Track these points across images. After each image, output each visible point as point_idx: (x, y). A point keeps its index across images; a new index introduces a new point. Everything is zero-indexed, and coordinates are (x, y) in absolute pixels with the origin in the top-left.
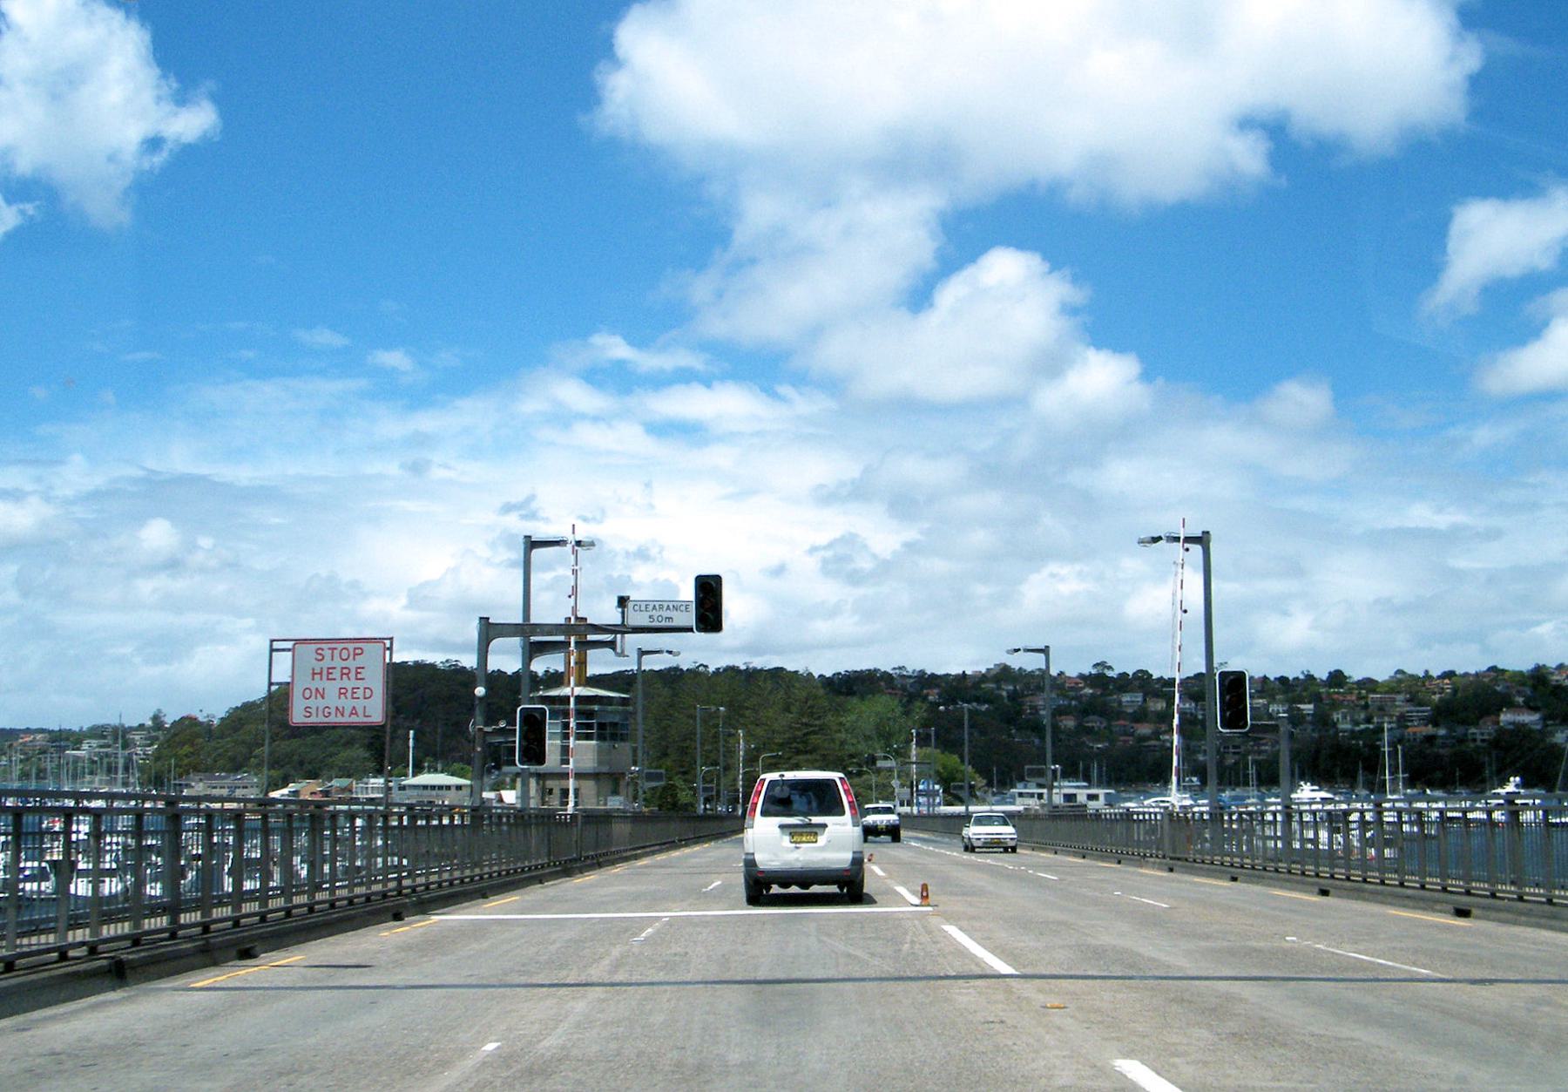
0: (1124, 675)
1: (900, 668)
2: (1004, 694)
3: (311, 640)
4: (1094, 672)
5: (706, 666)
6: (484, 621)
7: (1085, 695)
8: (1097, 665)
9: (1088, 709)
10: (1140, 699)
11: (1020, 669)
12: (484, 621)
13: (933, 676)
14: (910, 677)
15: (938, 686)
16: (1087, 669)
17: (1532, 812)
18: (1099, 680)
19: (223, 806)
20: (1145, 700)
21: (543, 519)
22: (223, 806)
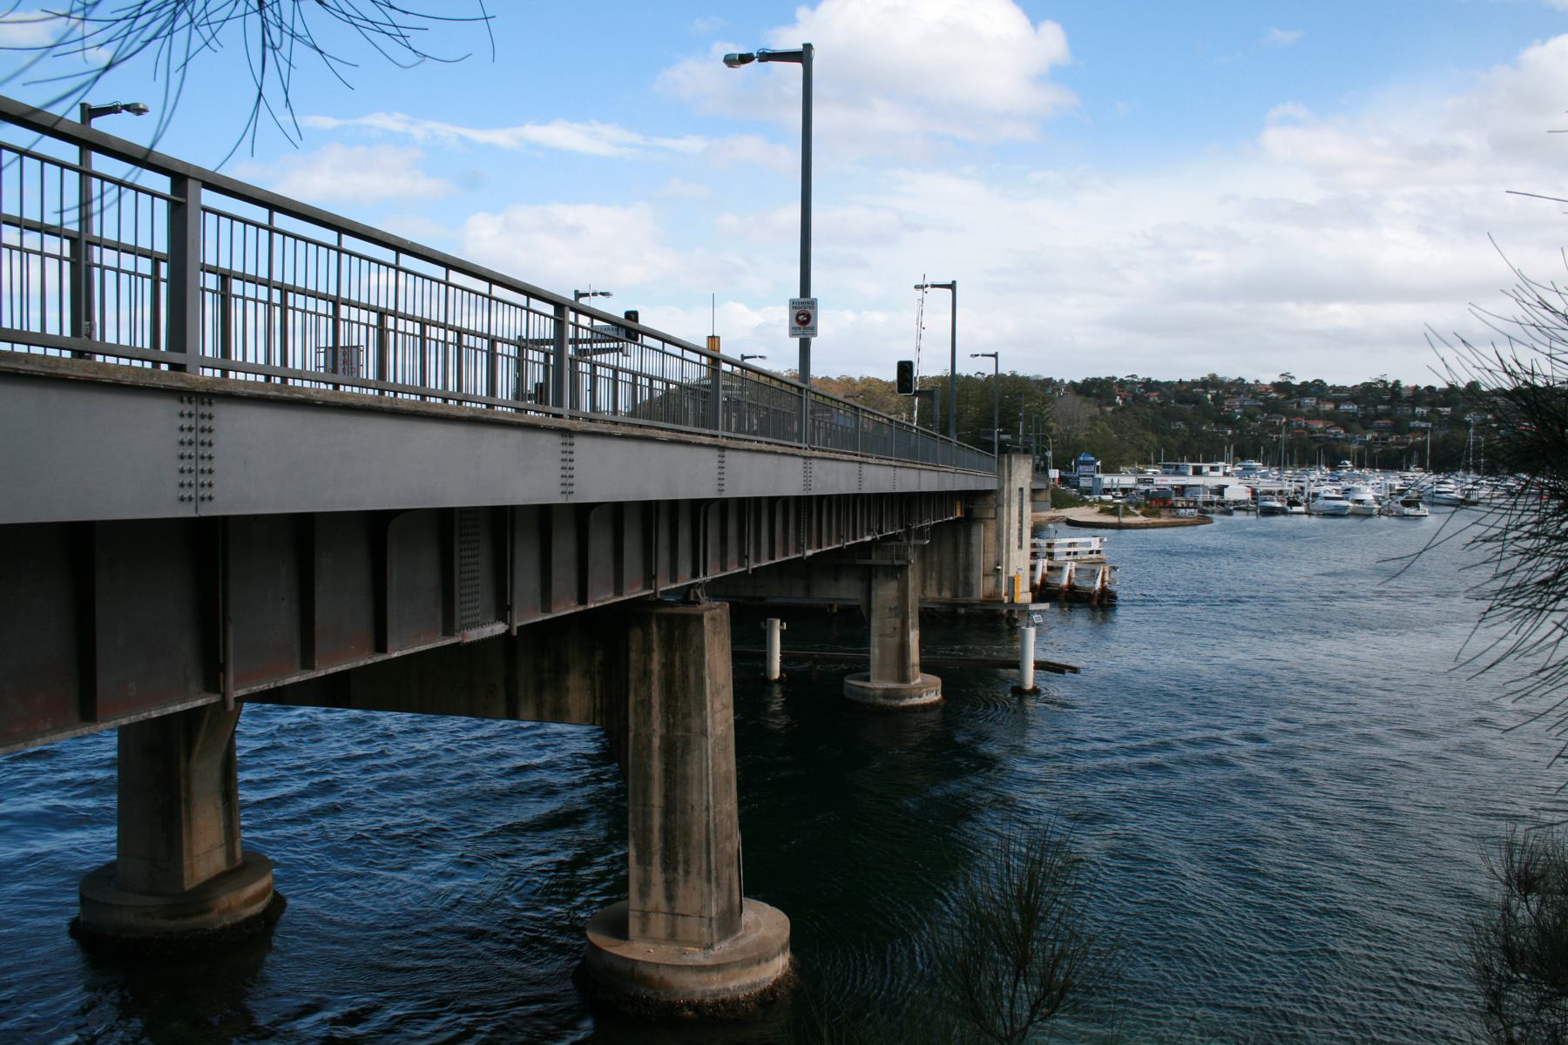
0: (1305, 384)
1: (1132, 376)
2: (1209, 396)
3: (610, 436)
4: (1280, 380)
5: (983, 374)
6: (576, 292)
7: (1271, 398)
8: (1283, 375)
9: (1272, 407)
10: (1314, 401)
11: (792, 335)
12: (576, 292)
13: (1157, 383)
14: (1139, 383)
15: (1159, 390)
16: (1277, 379)
17: (580, 337)
18: (1283, 387)
19: (164, 280)
20: (1317, 403)
21: (651, 938)
22: (164, 280)
